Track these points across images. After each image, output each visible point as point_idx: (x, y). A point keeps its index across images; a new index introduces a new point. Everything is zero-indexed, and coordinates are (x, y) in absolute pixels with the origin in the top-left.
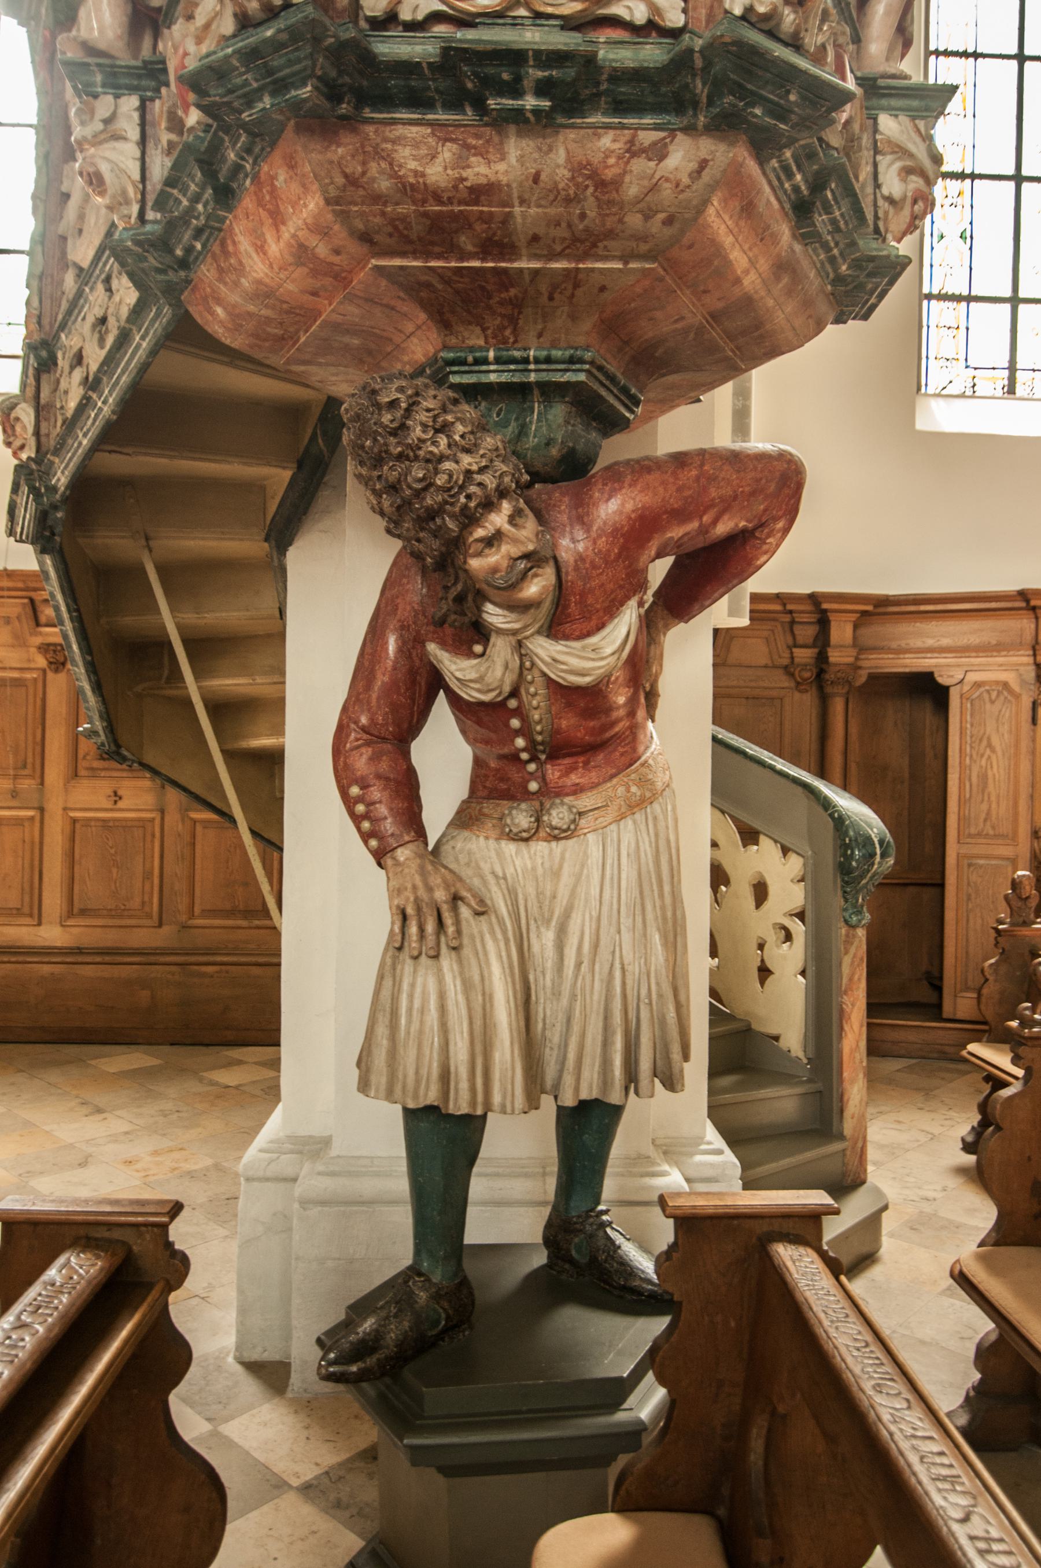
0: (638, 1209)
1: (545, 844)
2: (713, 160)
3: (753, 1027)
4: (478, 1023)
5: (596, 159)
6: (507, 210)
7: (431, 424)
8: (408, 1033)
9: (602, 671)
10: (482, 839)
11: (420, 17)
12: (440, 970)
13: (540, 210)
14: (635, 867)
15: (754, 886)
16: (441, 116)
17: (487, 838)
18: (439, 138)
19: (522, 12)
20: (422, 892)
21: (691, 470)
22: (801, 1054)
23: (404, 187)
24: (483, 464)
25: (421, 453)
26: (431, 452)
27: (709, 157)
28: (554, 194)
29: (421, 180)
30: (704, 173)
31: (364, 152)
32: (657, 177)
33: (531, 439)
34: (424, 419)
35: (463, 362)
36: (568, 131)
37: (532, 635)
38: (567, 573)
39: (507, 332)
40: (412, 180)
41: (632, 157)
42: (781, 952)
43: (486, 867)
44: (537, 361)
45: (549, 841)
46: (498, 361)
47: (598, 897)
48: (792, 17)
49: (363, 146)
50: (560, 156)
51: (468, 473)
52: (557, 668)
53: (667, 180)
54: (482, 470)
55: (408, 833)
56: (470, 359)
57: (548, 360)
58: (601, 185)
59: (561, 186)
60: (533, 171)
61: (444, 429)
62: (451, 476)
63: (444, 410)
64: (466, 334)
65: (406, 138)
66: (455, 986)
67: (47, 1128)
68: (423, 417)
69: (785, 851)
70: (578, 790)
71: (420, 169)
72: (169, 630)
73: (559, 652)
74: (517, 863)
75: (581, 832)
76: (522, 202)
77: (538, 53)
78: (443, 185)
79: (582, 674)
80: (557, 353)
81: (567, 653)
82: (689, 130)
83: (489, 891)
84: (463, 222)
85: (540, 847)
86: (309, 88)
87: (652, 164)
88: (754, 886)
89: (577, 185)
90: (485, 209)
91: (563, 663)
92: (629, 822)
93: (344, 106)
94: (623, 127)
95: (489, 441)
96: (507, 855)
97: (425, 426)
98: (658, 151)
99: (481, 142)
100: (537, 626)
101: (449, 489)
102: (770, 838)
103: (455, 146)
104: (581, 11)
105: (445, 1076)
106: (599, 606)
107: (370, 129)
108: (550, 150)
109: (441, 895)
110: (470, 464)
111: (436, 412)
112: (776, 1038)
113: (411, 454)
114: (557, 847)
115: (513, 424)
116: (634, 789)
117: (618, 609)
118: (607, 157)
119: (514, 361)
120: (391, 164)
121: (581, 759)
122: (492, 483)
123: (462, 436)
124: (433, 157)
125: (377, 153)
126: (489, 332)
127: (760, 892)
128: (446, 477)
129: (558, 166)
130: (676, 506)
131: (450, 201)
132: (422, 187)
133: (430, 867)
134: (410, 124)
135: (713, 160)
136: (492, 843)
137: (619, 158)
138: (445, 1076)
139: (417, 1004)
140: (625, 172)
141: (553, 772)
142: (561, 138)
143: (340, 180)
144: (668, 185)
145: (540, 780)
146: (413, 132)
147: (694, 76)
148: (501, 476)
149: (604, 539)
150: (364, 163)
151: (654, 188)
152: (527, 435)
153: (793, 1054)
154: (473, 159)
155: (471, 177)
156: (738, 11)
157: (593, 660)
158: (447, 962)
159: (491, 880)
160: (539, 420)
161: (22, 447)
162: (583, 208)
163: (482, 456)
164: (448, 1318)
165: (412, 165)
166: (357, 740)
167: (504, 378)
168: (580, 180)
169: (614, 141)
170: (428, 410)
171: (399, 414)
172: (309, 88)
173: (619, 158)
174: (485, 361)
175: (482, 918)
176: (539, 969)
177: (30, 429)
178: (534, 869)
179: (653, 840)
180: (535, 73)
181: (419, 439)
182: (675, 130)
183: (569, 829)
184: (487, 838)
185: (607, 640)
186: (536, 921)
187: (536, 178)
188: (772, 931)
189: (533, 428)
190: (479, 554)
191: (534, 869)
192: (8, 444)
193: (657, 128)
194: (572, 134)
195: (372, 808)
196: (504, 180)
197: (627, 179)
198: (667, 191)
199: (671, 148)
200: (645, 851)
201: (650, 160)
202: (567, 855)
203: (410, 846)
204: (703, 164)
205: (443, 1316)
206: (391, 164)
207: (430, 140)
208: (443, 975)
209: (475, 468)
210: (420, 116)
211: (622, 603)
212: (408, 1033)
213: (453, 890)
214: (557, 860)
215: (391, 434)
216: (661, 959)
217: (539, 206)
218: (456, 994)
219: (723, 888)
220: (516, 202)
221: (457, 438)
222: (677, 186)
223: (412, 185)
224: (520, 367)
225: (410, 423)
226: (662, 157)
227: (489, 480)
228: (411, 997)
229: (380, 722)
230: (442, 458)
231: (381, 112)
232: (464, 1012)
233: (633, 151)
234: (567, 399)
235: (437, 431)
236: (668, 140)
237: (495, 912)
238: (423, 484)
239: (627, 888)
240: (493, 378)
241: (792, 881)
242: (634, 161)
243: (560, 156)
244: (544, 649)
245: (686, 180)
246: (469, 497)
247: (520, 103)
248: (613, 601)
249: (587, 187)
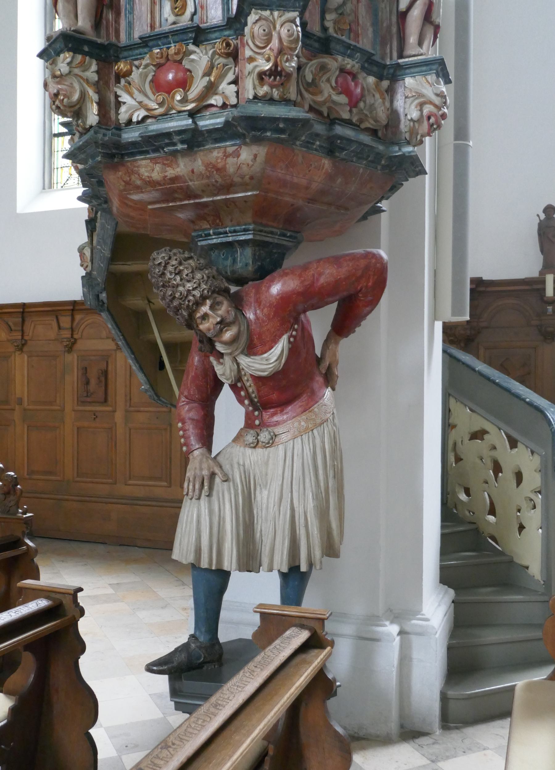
0: (367, 642)
1: (261, 449)
2: (259, 154)
3: (514, 560)
4: (215, 529)
5: (213, 161)
6: (187, 184)
7: (173, 271)
8: (185, 531)
9: (272, 369)
10: (238, 447)
11: (140, 119)
12: (199, 505)
13: (199, 182)
14: (301, 461)
15: (516, 473)
16: (152, 155)
17: (240, 447)
18: (153, 163)
19: (174, 111)
20: (198, 472)
21: (310, 271)
22: (539, 578)
23: (146, 182)
24: (195, 286)
25: (170, 284)
26: (173, 284)
27: (257, 153)
28: (201, 176)
29: (151, 179)
30: (257, 159)
31: (129, 173)
32: (239, 163)
33: (239, 264)
34: (171, 270)
35: (201, 236)
36: (200, 152)
37: (238, 354)
38: (252, 325)
39: (218, 221)
40: (148, 180)
41: (226, 158)
42: (529, 514)
43: (235, 461)
44: (230, 232)
45: (263, 448)
46: (215, 234)
47: (281, 475)
48: (277, 92)
49: (128, 171)
50: (199, 162)
51: (189, 291)
52: (251, 369)
53: (243, 164)
54: (194, 289)
55: (198, 444)
56: (203, 235)
57: (235, 231)
58: (218, 170)
59: (203, 172)
60: (191, 169)
61: (179, 273)
62: (181, 294)
63: (180, 264)
64: (201, 224)
65: (142, 165)
66: (205, 512)
67: (155, 590)
68: (170, 268)
69: (532, 452)
70: (277, 424)
71: (149, 175)
72: (158, 343)
73: (249, 362)
74: (252, 458)
75: (276, 444)
76: (191, 180)
77: (174, 132)
78: (159, 179)
79: (263, 371)
80: (238, 228)
81: (253, 362)
82: (245, 144)
83: (233, 471)
84: (174, 191)
85: (259, 451)
86: (100, 157)
87: (236, 159)
88: (516, 473)
89: (209, 171)
90: (178, 185)
91: (253, 367)
92: (299, 439)
93: (116, 159)
94: (219, 147)
95: (198, 276)
96: (247, 454)
97: (171, 273)
98: (237, 154)
99: (169, 162)
100: (240, 350)
101: (181, 299)
102: (524, 444)
103: (160, 165)
104: (195, 106)
105: (198, 551)
106: (268, 339)
107: (129, 164)
108: (195, 160)
109: (205, 473)
110: (189, 287)
111: (176, 266)
112: (527, 568)
113: (167, 285)
114: (266, 451)
115: (230, 258)
116: (303, 423)
117: (278, 340)
118: (217, 159)
119: (221, 233)
120: (139, 175)
121: (279, 409)
122: (198, 294)
123: (187, 275)
124: (153, 170)
125: (133, 172)
126: (210, 222)
127: (519, 477)
128: (179, 294)
129: (199, 166)
130: (300, 290)
131: (164, 184)
132: (152, 181)
133: (205, 460)
134: (142, 160)
135: (259, 154)
136: (242, 448)
137: (222, 159)
138: (198, 551)
139: (189, 520)
140: (226, 164)
141: (266, 415)
142: (198, 155)
143: (123, 183)
144: (244, 166)
145: (260, 419)
146: (144, 162)
147: (236, 127)
148: (203, 290)
149: (266, 309)
150: (129, 176)
151: (239, 168)
152: (237, 263)
153: (536, 578)
154: (167, 169)
155: (168, 175)
156: (251, 97)
157: (266, 364)
158: (204, 501)
159: (236, 466)
160: (241, 255)
161: (87, 266)
162: (215, 179)
163: (194, 283)
164: (205, 657)
165: (146, 174)
166: (183, 402)
167: (219, 241)
168: (209, 169)
169: (218, 153)
170: (173, 266)
171: (162, 268)
172: (100, 157)
173: (222, 159)
174: (209, 235)
175: (225, 483)
176: (259, 508)
177: (89, 258)
178: (258, 461)
179: (312, 448)
180: (176, 138)
181: (169, 279)
182: (241, 145)
183: (268, 443)
184: (240, 447)
185: (272, 355)
186: (260, 485)
187: (193, 171)
188: (525, 502)
189: (239, 259)
190: (201, 323)
191: (258, 461)
192: (82, 265)
193: (233, 145)
194: (202, 154)
195: (185, 432)
196: (181, 174)
197: (227, 166)
198: (245, 168)
199: (241, 152)
200: (307, 454)
201: (234, 158)
202: (271, 455)
203: (199, 450)
204: (255, 156)
205: (203, 656)
206: (139, 175)
207: (150, 164)
208: (201, 507)
209: (191, 288)
210: (144, 157)
211: (280, 337)
212: (185, 531)
213: (212, 470)
214: (266, 457)
215: (160, 277)
216: (312, 505)
217: (198, 181)
218: (205, 516)
219: (500, 474)
220: (189, 181)
221: (185, 276)
222: (248, 165)
223: (148, 181)
224: (225, 235)
225: (166, 272)
226: (238, 156)
227: (197, 293)
228: (187, 516)
229: (192, 394)
230: (178, 285)
231: (131, 157)
232: (208, 524)
233: (226, 156)
234: (250, 245)
235: (176, 274)
236: (239, 149)
237: (233, 480)
238: (172, 297)
239: (296, 471)
240: (215, 241)
241: (535, 471)
242: (228, 159)
243: (199, 162)
244: (244, 361)
245: (251, 163)
246: (189, 301)
247: (176, 148)
248: (275, 336)
249: (213, 172)
